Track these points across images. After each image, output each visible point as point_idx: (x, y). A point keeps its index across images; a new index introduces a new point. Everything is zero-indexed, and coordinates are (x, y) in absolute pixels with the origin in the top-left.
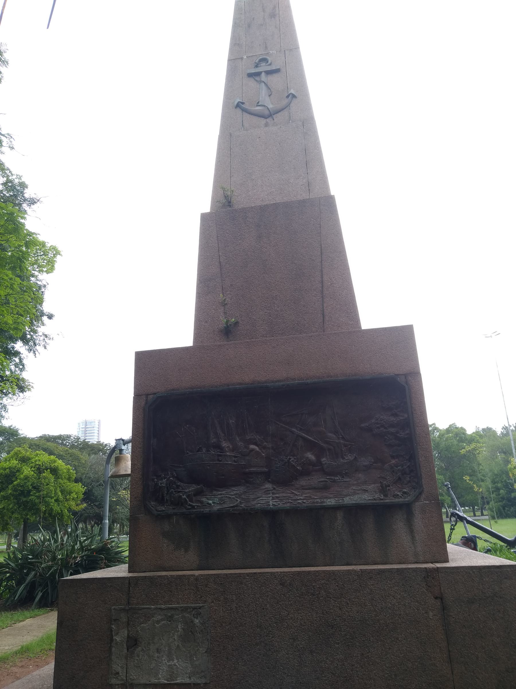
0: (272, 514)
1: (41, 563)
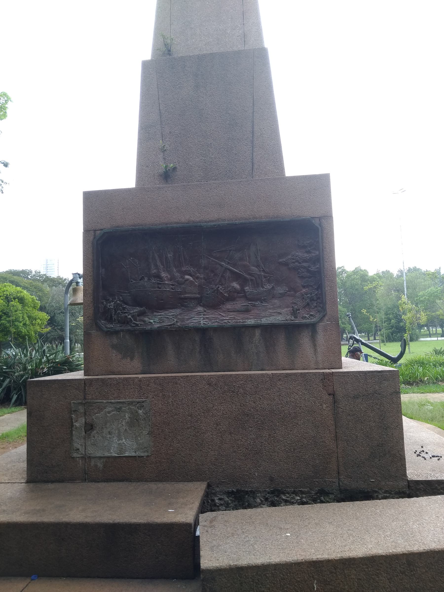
0: (203, 331)
1: (15, 373)
